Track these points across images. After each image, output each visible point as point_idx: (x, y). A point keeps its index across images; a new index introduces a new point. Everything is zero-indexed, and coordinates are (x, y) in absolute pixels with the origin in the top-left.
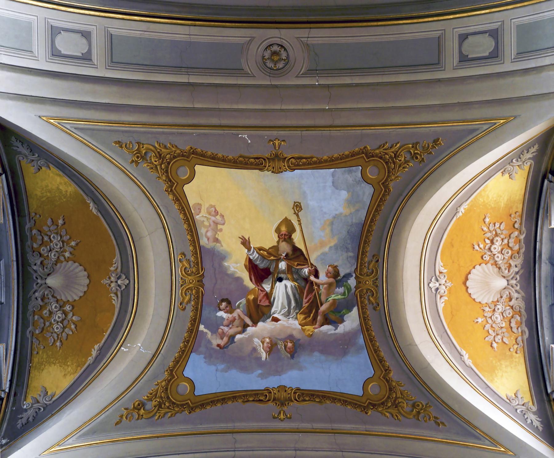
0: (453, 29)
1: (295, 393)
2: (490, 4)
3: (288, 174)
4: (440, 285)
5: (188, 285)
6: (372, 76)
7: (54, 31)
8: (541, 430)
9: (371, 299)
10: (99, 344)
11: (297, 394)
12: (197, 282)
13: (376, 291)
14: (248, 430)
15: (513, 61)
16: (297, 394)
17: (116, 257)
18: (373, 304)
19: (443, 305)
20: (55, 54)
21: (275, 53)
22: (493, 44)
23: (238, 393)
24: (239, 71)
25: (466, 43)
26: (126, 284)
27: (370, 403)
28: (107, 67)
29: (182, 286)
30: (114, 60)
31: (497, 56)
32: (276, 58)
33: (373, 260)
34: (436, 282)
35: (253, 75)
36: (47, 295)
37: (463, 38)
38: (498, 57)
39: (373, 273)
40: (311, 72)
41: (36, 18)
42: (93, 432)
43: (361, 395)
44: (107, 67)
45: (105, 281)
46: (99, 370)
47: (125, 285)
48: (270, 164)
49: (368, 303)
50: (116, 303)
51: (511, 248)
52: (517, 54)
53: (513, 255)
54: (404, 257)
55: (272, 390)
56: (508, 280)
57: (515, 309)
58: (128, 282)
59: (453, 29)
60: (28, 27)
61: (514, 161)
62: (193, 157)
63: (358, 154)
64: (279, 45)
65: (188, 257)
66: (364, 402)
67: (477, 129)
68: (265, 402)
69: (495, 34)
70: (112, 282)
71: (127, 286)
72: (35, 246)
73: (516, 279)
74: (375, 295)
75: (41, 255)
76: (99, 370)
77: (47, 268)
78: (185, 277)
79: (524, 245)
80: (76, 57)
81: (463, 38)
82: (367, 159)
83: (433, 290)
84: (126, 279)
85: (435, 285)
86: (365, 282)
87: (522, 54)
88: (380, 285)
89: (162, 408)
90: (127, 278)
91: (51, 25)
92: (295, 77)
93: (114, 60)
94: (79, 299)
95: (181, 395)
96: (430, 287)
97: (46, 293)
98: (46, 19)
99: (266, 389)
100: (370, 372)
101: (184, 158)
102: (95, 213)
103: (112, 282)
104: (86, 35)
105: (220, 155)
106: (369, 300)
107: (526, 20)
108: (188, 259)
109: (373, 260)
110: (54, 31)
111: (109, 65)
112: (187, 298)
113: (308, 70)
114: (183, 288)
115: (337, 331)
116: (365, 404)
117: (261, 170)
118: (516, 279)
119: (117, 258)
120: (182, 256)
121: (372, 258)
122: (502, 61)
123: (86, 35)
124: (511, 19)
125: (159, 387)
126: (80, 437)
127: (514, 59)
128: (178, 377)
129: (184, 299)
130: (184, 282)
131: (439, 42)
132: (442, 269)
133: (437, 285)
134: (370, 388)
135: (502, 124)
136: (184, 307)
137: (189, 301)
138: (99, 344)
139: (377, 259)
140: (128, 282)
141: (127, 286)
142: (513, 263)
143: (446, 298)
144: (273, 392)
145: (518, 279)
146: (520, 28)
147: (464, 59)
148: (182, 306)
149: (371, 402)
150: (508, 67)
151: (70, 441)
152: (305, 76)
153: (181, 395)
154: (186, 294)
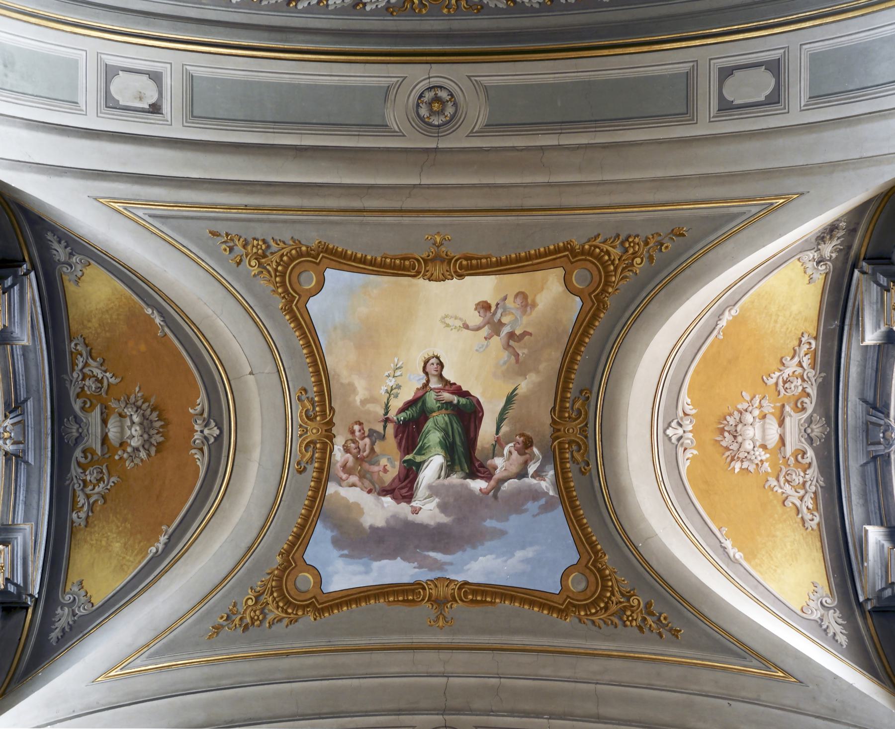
0: (710, 59)
1: (460, 588)
2: (761, 23)
4: (684, 432)
6: (525, 136)
7: (110, 73)
8: (845, 644)
9: (575, 454)
11: (464, 590)
13: (584, 443)
15: (802, 108)
16: (464, 590)
17: (686, 468)
20: (110, 103)
21: (437, 99)
22: (773, 82)
24: (382, 128)
25: (730, 82)
28: (185, 124)
29: (301, 436)
30: (195, 114)
31: (777, 100)
32: (436, 106)
34: (679, 428)
35: (403, 133)
37: (726, 73)
38: (779, 103)
39: (580, 416)
40: (493, 127)
41: (84, 53)
42: (171, 649)
43: (558, 592)
44: (185, 124)
47: (215, 437)
50: (202, 464)
52: (810, 98)
55: (426, 583)
58: (218, 432)
59: (710, 59)
60: (73, 64)
64: (430, 89)
65: (310, 395)
68: (419, 603)
69: (775, 67)
71: (219, 438)
74: (305, 410)
80: (140, 110)
81: (726, 73)
83: (674, 440)
84: (216, 428)
85: (677, 432)
87: (817, 98)
88: (590, 434)
91: (106, 64)
92: (467, 136)
93: (195, 114)
96: (668, 435)
98: (99, 55)
100: (573, 557)
104: (156, 77)
107: (819, 47)
108: (310, 397)
110: (110, 73)
111: (188, 120)
112: (309, 455)
113: (485, 126)
114: (304, 440)
115: (126, 427)
119: (297, 412)
121: (577, 394)
122: (786, 111)
123: (156, 77)
124: (801, 45)
126: (149, 657)
127: (805, 106)
129: (303, 456)
131: (688, 79)
132: (690, 410)
133: (680, 431)
136: (303, 467)
139: (586, 394)
140: (218, 432)
141: (219, 438)
143: (695, 452)
146: (815, 58)
147: (726, 107)
148: (299, 467)
149: (571, 601)
150: (795, 117)
151: (138, 661)
152: (480, 133)
154: (306, 450)
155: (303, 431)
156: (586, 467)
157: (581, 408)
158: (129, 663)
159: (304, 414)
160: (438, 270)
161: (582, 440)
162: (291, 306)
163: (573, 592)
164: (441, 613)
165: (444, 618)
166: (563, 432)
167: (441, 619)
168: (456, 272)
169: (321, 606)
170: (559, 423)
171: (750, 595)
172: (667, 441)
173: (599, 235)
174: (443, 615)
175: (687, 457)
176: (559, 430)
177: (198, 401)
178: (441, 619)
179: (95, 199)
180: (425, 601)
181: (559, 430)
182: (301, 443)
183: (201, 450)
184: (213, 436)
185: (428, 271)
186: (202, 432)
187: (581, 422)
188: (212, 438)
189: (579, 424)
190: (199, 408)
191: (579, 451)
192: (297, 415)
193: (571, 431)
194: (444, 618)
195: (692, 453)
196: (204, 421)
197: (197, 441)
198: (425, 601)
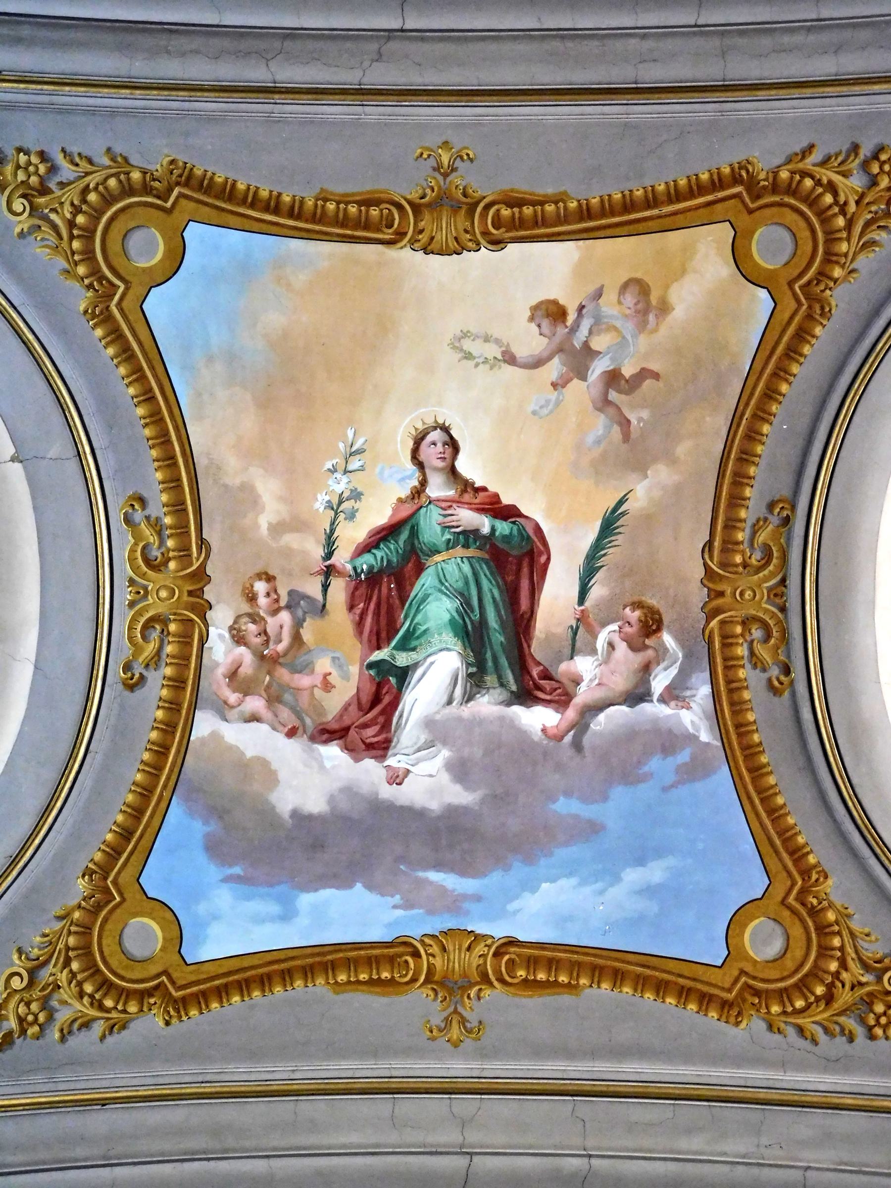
1: (497, 954)
11: (507, 957)
12: (186, 594)
14: (433, 1083)
16: (507, 957)
27: (747, 986)
29: (132, 604)
33: (770, 517)
39: (768, 563)
54: (874, 608)
55: (422, 942)
62: (729, 990)
66: (727, 985)
78: (143, 576)
95: (123, 952)
101: (150, 199)
109: (770, 517)
112: (150, 648)
114: (139, 613)
116: (181, 195)
120: (132, 505)
128: (123, 899)
129: (138, 650)
137: (156, 659)
144: (426, 951)
153: (123, 952)
154: (144, 637)
161: (773, 615)
164: (456, 1011)
165: (463, 1021)
168: (485, 233)
170: (193, 608)
176: (721, 594)
181: (721, 594)
182: (134, 620)
185: (421, 232)
187: (772, 575)
192: (122, 554)
193: (748, 594)
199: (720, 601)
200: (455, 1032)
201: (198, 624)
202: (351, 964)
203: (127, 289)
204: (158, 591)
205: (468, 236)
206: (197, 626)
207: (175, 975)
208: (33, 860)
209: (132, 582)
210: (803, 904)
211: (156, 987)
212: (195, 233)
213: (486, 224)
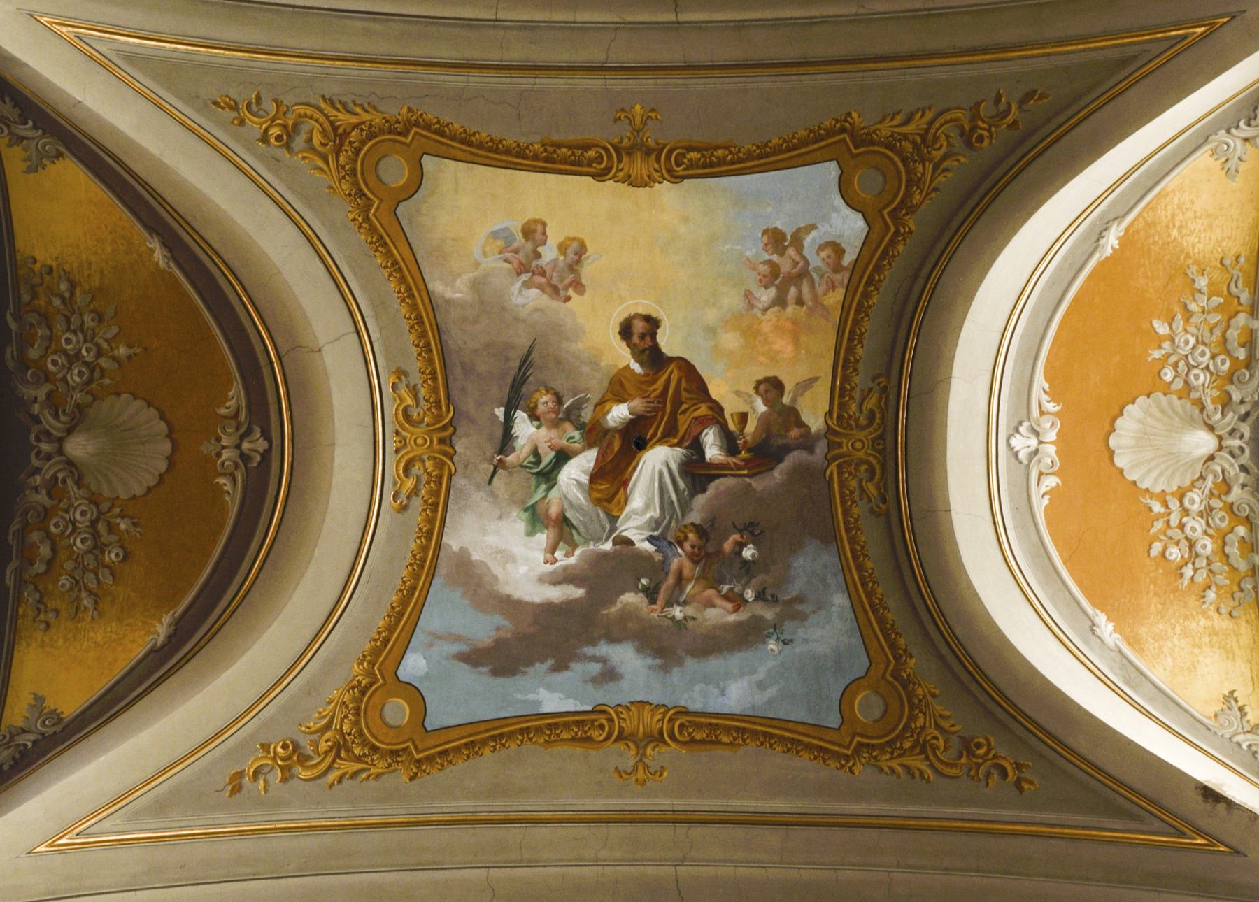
1: (608, 169)
3: (666, 192)
5: (412, 450)
10: (172, 612)
18: (870, 501)
19: (1046, 501)
23: (738, 169)
26: (1018, 436)
29: (397, 451)
36: (64, 481)
45: (208, 448)
46: (1085, 219)
48: (620, 167)
49: (419, 386)
51: (49, 536)
53: (41, 518)
56: (1220, 438)
57: (1238, 510)
58: (265, 445)
61: (1242, 124)
63: (831, 132)
67: (1135, 57)
70: (224, 447)
71: (266, 455)
72: (1241, 530)
73: (1242, 437)
75: (48, 377)
76: (1085, 219)
77: (64, 411)
79: (11, 542)
82: (856, 148)
86: (852, 445)
89: (918, 134)
90: (266, 435)
94: (1137, 397)
97: (1219, 416)
99: (679, 180)
102: (162, 264)
103: (224, 447)
105: (509, 141)
106: (416, 397)
117: (683, 710)
118: (1242, 437)
125: (930, 185)
128: (880, 211)
130: (403, 442)
134: (860, 705)
135: (1204, 36)
137: (415, 492)
138: (172, 612)
140: (265, 445)
141: (266, 455)
142: (42, 498)
144: (619, 723)
145: (1247, 435)
155: (400, 442)
156: (881, 505)
157: (404, 479)
158: (1170, 48)
159: (400, 412)
160: (638, 167)
161: (875, 457)
162: (368, 215)
163: (398, 153)
164: (641, 760)
165: (646, 767)
166: (845, 449)
167: (638, 120)
168: (670, 171)
169: (422, 755)
170: (445, 454)
171: (1138, 707)
172: (1013, 460)
173: (361, 782)
174: (644, 762)
175: (234, 400)
176: (441, 441)
177: (231, 393)
178: (638, 120)
179: (1238, 852)
180: (667, 148)
182: (399, 462)
183: (1042, 413)
184: (258, 452)
185: (621, 170)
186: (238, 447)
188: (1023, 433)
189: (871, 433)
190: (232, 403)
191: (871, 479)
192: (391, 410)
193: (420, 441)
194: (646, 767)
195: (227, 408)
196: (1039, 461)
197: (226, 464)
198: (667, 148)
199: (443, 434)
200: (641, 774)
201: (449, 466)
202: (722, 161)
203: (884, 675)
204: (863, 447)
205: (623, 716)
206: (446, 468)
207: (417, 743)
208: (327, 640)
209: (397, 433)
210: (368, 199)
211: (404, 750)
212: (833, 720)
213: (609, 727)
